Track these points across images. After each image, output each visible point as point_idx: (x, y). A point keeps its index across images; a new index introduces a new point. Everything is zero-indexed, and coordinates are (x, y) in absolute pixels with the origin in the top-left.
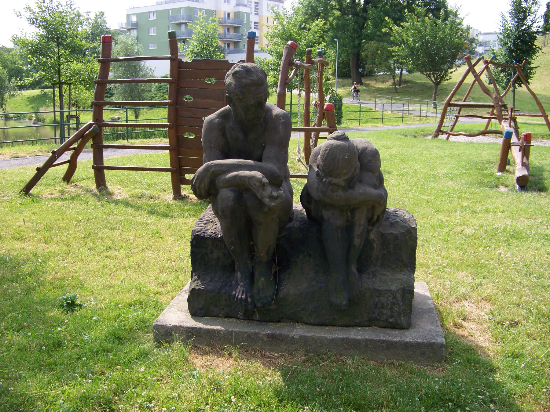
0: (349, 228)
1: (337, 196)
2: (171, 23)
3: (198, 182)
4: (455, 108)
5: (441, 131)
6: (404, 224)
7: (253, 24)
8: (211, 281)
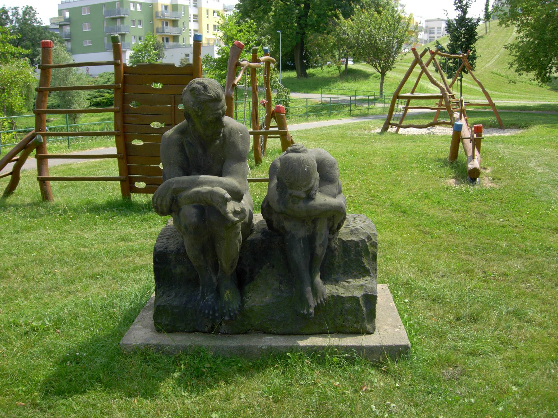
0: (311, 240)
1: (298, 207)
2: (106, 17)
3: (159, 199)
4: (403, 100)
5: (390, 124)
6: (364, 231)
7: (192, 17)
8: (176, 296)
